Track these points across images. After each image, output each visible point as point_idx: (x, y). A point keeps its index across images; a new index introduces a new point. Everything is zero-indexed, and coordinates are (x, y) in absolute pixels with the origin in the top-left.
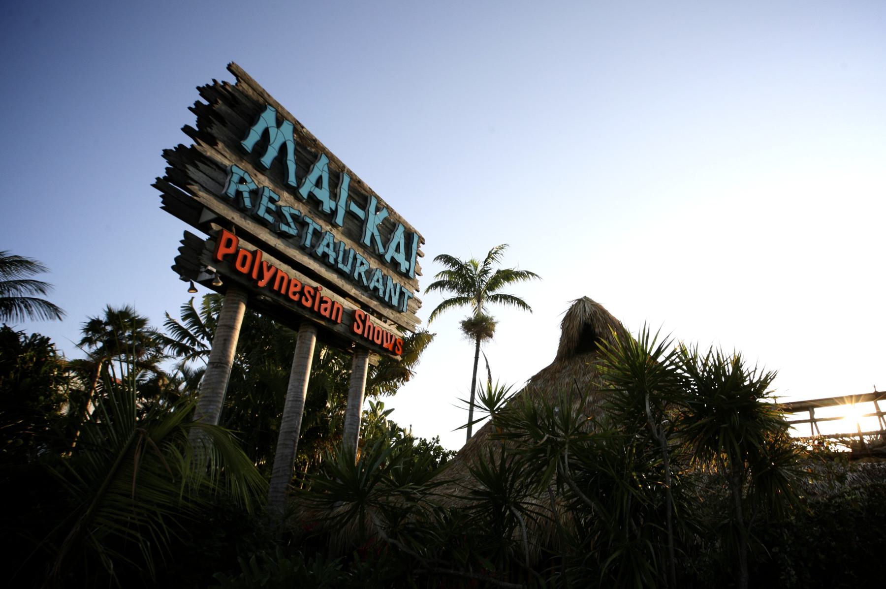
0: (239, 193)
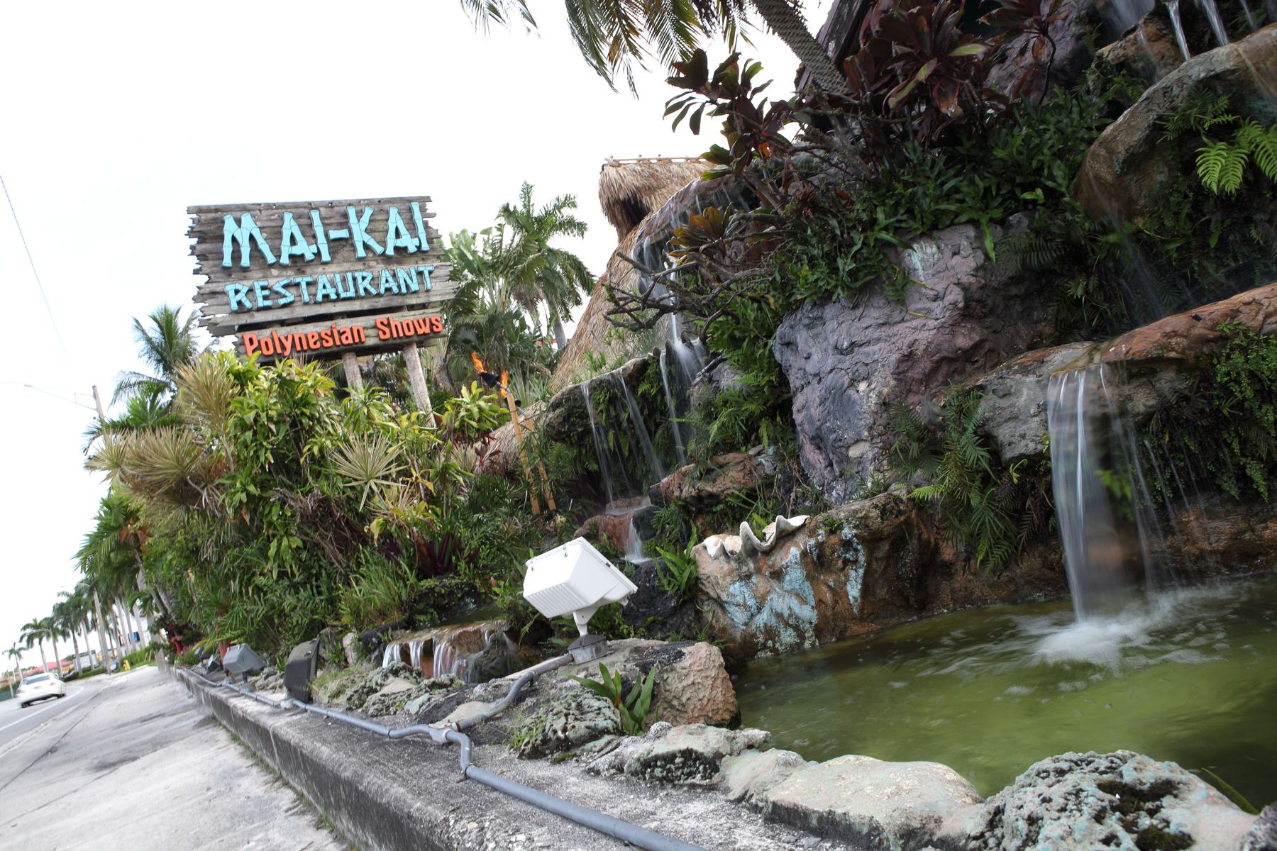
0: (239, 303)
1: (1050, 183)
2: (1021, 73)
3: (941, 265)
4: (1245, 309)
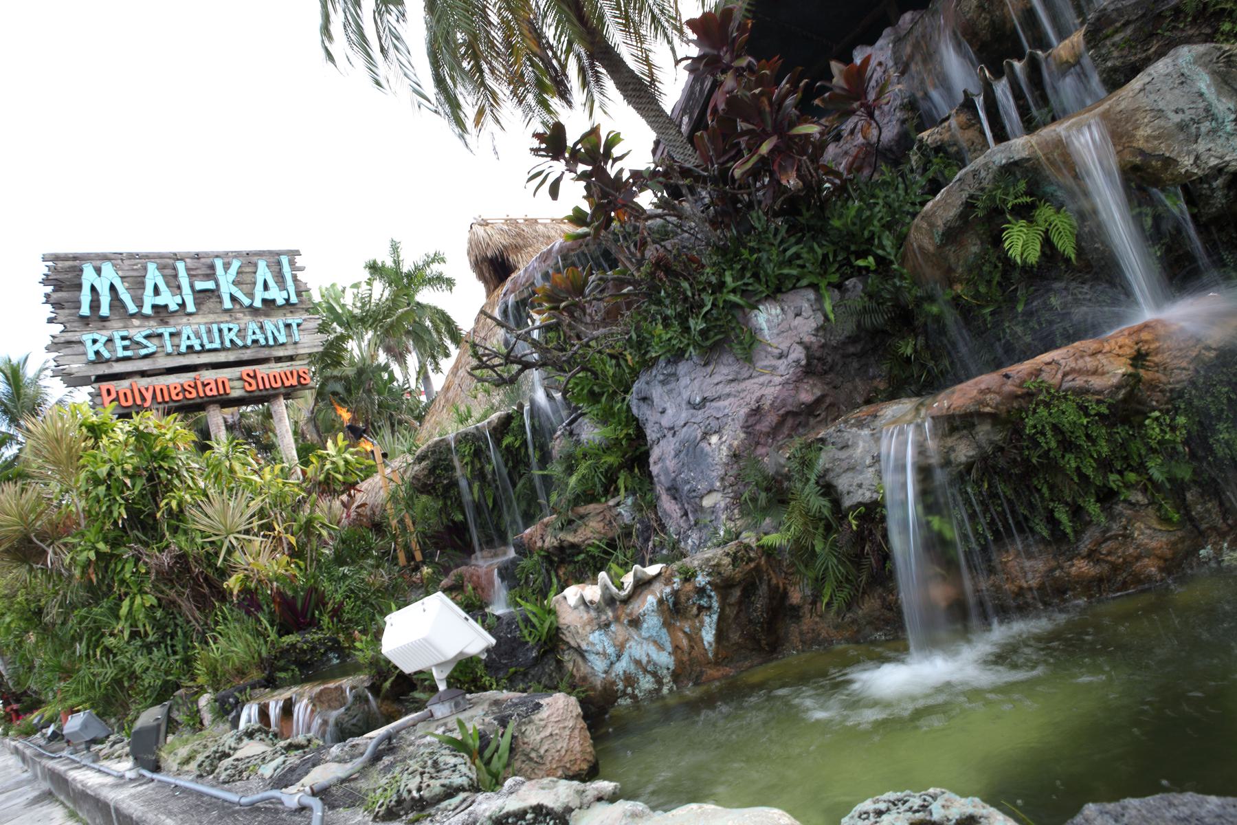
1: (880, 252)
3: (785, 325)
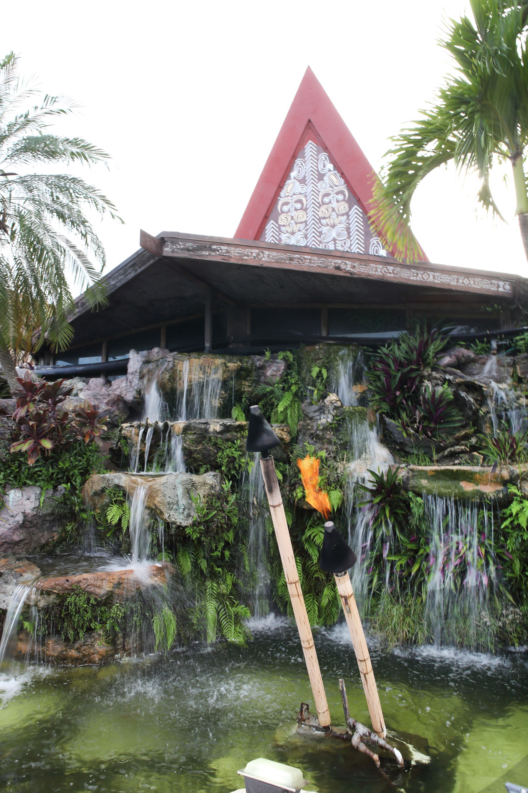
1: (74, 483)
2: (113, 396)
3: (20, 502)
4: (83, 581)
